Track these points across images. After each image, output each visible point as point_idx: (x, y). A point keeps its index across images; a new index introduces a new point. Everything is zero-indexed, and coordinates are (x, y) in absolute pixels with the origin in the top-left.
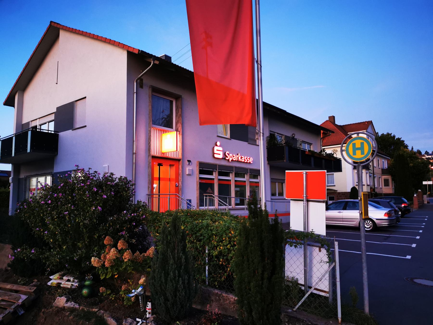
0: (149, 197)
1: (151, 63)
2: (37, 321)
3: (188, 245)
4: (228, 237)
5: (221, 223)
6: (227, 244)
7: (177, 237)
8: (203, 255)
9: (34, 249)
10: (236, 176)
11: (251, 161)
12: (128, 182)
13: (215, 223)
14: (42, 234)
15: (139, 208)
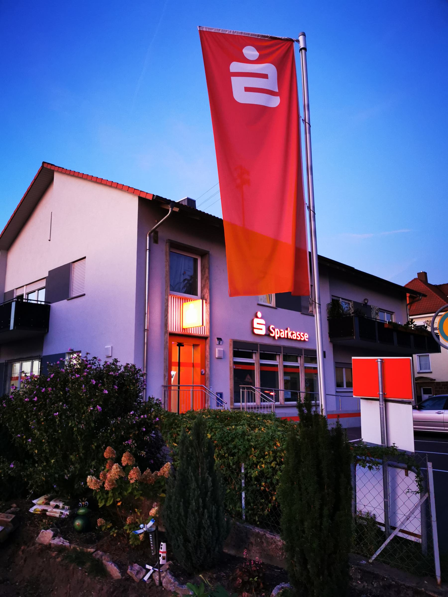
0: (165, 389)
1: (169, 210)
2: (14, 562)
3: (217, 460)
4: (272, 451)
5: (262, 429)
6: (271, 461)
7: (201, 449)
8: (238, 475)
9: (13, 462)
10: (285, 359)
11: (307, 338)
12: (137, 371)
13: (254, 429)
14: (24, 442)
15: (151, 406)
